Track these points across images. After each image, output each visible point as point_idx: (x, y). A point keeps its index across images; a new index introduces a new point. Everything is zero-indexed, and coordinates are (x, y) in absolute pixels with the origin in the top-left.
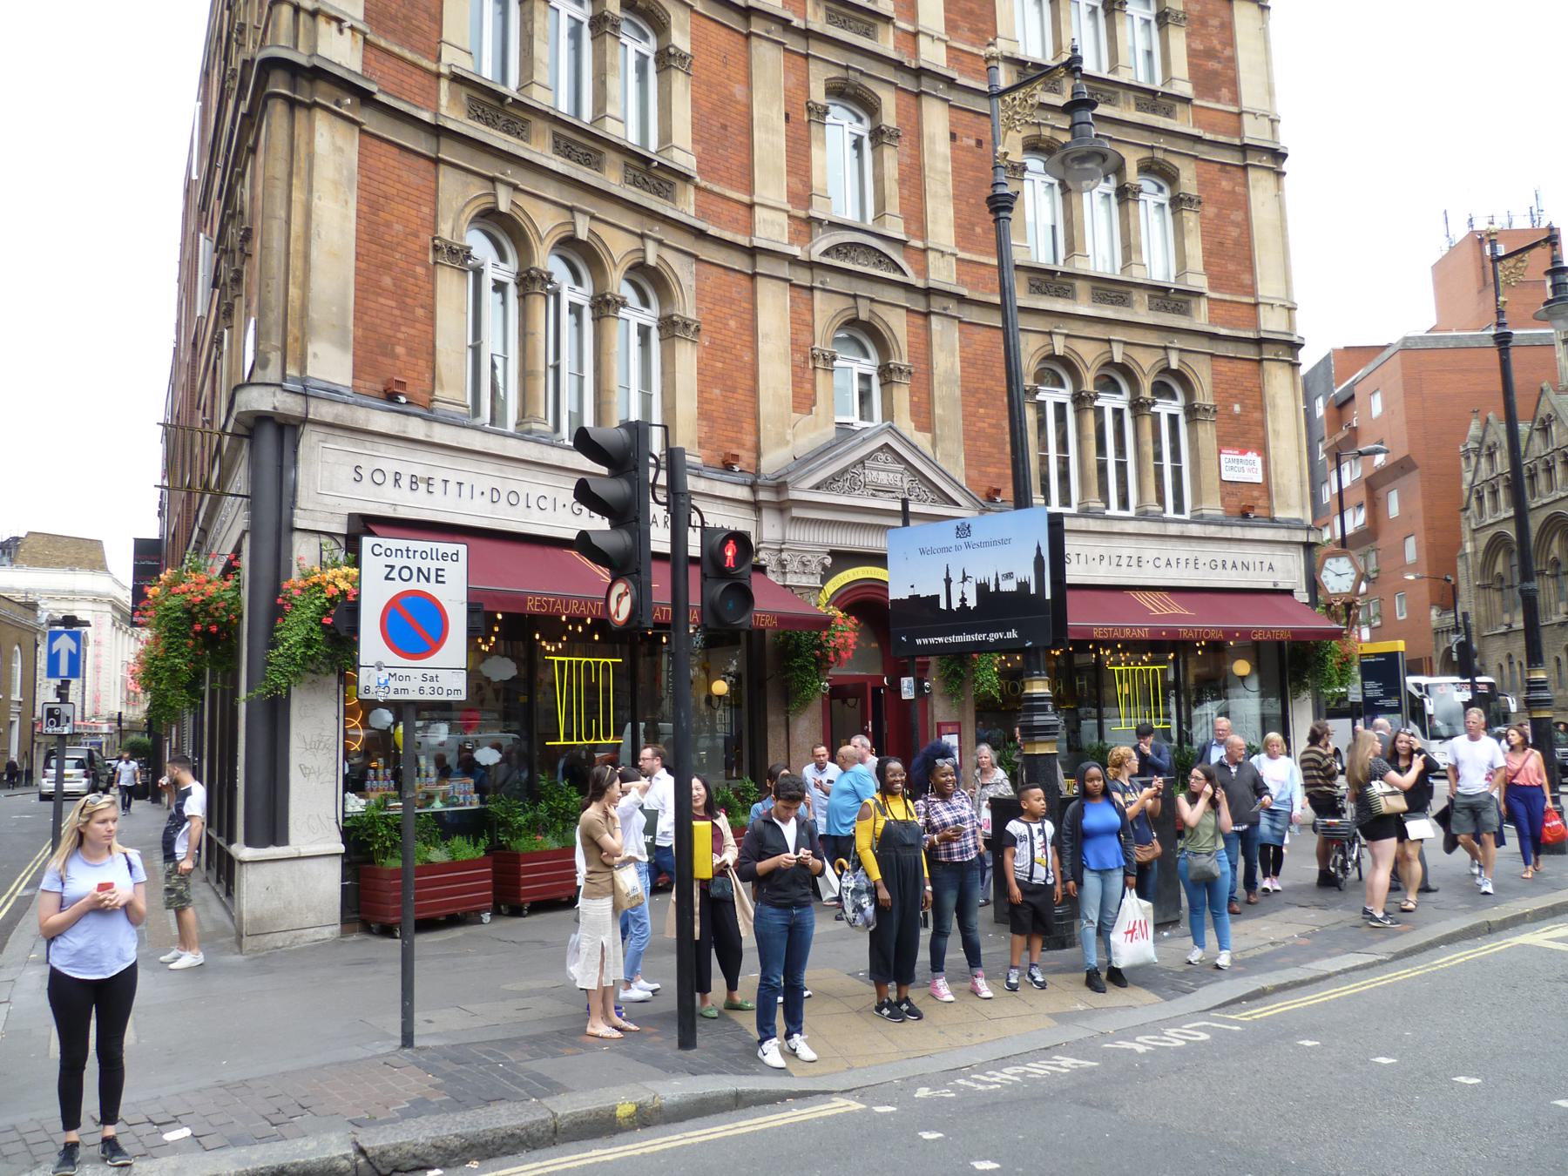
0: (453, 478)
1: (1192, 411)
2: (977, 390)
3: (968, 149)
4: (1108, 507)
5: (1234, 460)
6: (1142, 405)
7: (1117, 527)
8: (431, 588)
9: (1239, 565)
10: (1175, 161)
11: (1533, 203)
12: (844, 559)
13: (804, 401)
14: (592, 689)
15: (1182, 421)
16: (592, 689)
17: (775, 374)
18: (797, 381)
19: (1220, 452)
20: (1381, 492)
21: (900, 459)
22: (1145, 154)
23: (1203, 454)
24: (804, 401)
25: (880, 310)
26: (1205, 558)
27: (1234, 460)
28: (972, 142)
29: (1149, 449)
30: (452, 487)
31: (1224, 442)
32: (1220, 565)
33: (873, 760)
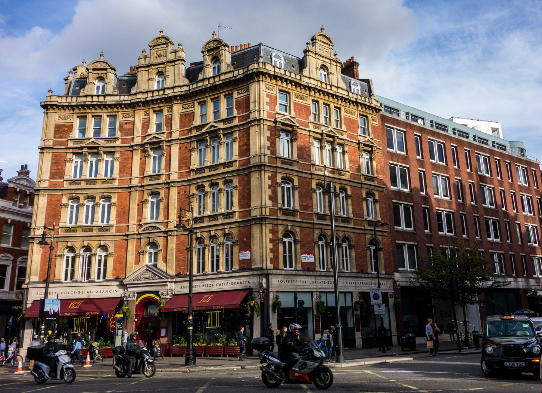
0: (309, 280)
1: (295, 241)
2: (180, 250)
3: (183, 194)
4: (372, 271)
5: (243, 254)
6: (328, 244)
7: (346, 275)
8: (377, 293)
9: (105, 291)
10: (293, 177)
11: (116, 73)
12: (140, 294)
13: (137, 261)
14: (215, 317)
15: (324, 246)
16: (215, 317)
17: (131, 257)
18: (136, 258)
19: (239, 252)
20: (378, 253)
21: (150, 271)
22: (318, 181)
23: (297, 254)
24: (137, 261)
25: (155, 239)
26: (215, 287)
27: (243, 254)
28: (183, 193)
29: (341, 255)
30: (293, 281)
31: (241, 250)
32: (81, 292)
33: (161, 339)
